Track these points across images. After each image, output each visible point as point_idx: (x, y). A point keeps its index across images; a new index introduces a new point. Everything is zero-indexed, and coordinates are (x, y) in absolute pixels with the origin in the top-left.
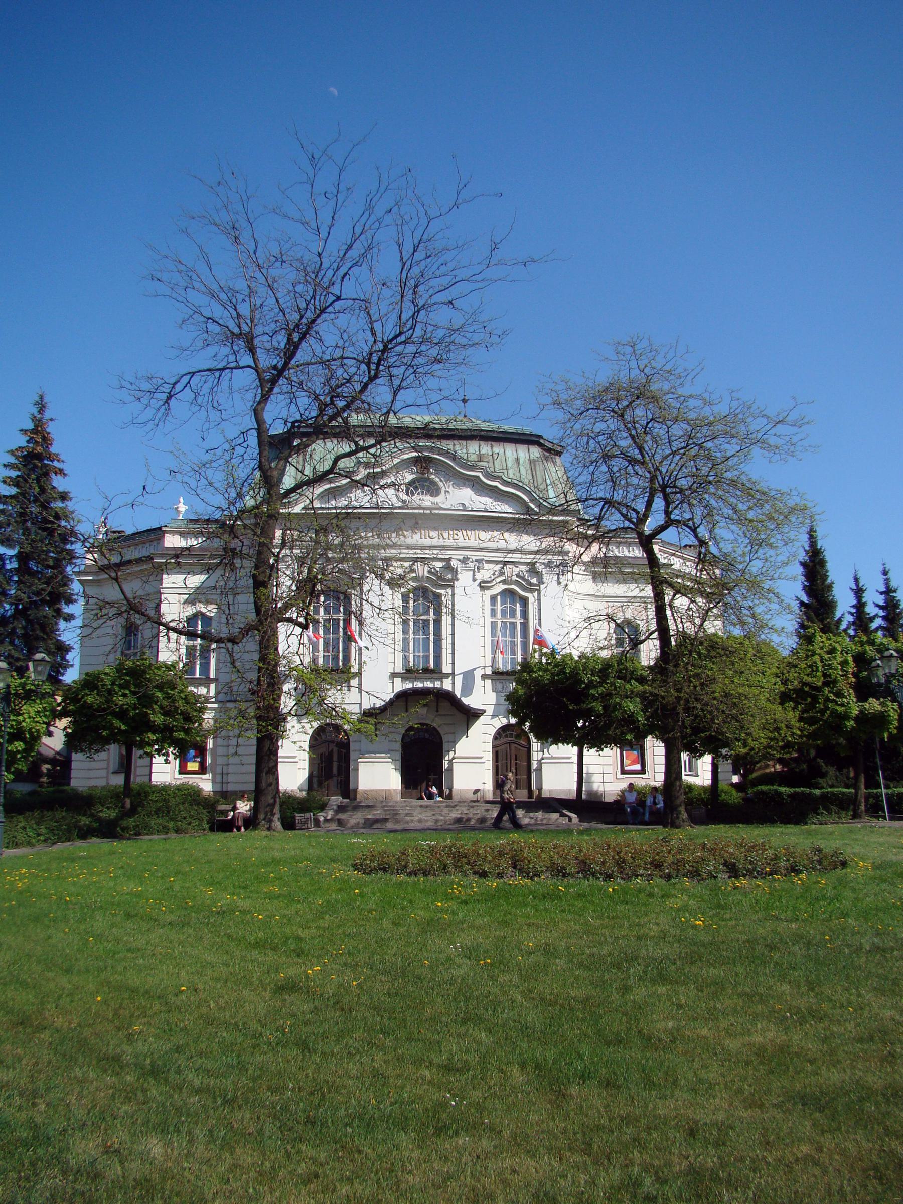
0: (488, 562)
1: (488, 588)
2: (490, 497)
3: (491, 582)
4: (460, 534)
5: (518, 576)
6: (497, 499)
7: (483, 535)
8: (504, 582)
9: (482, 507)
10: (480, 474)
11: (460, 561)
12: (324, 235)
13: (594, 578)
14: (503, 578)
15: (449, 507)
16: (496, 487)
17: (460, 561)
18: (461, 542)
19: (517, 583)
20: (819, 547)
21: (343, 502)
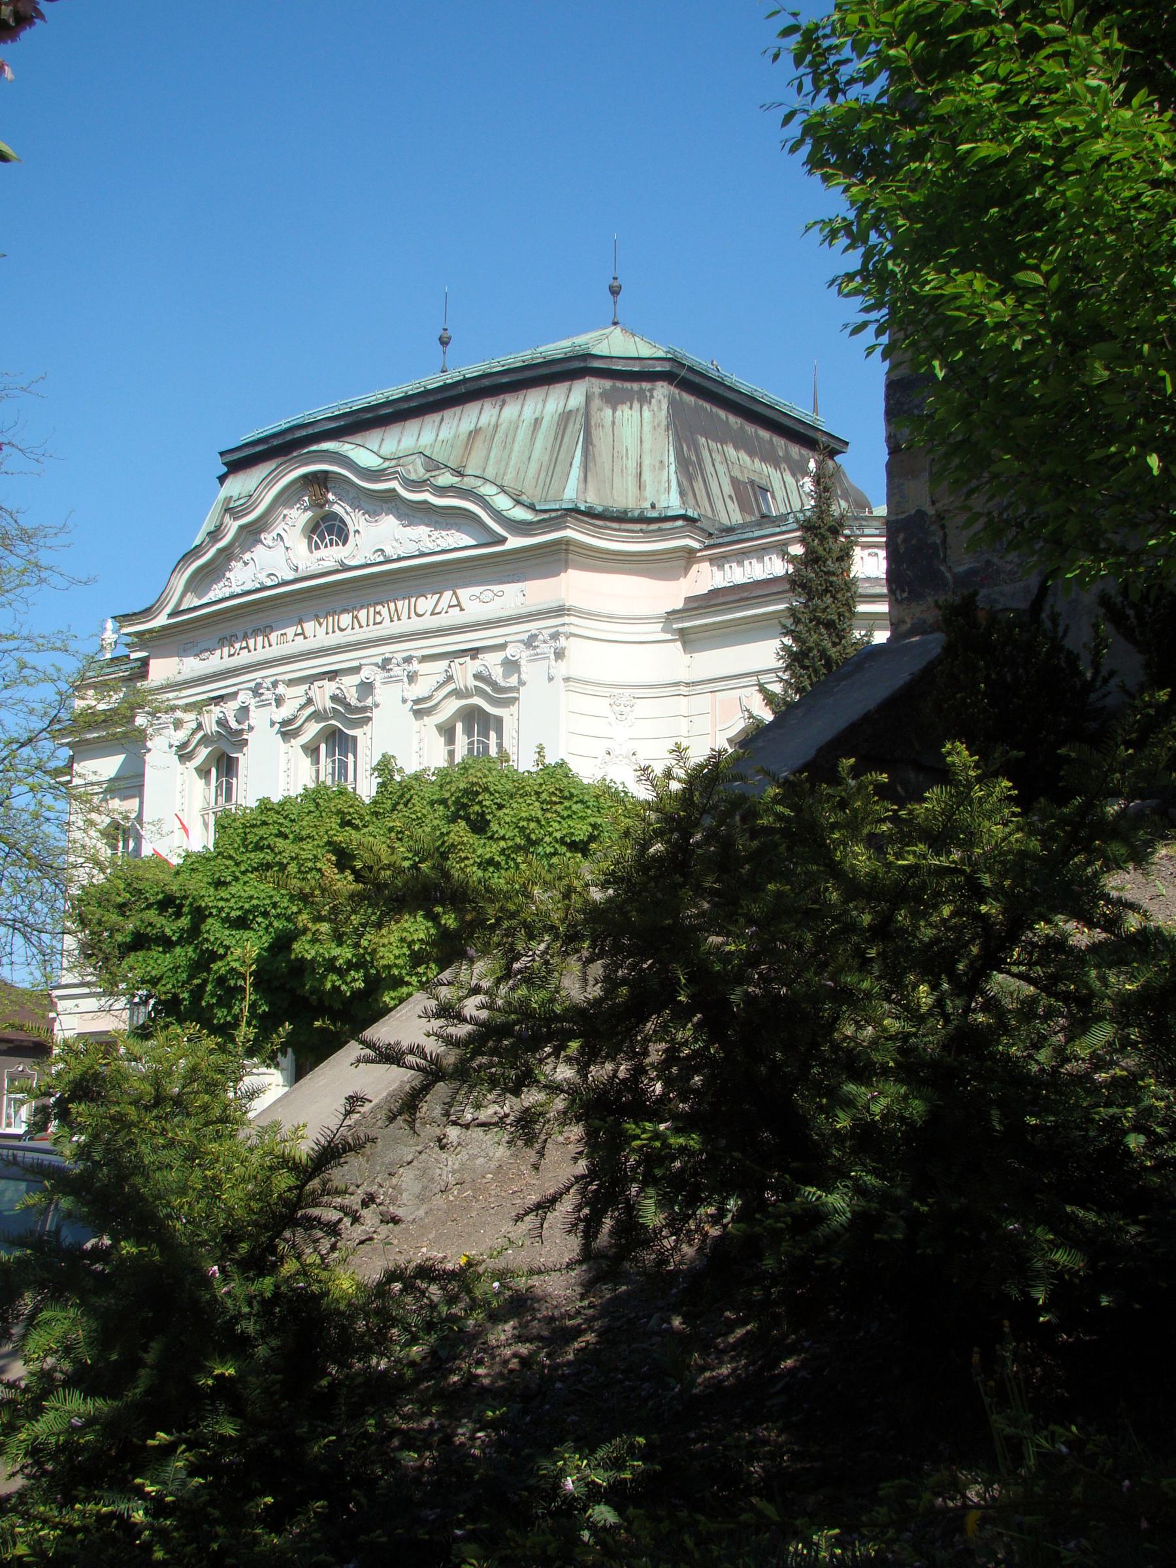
0: (425, 659)
1: (428, 712)
2: (428, 525)
3: (430, 697)
4: (385, 611)
5: (477, 677)
6: (437, 525)
7: (425, 604)
8: (457, 694)
9: (412, 549)
10: (394, 484)
11: (376, 665)
12: (727, 499)
13: (685, 645)
14: (311, 709)
15: (362, 562)
16: (426, 502)
17: (376, 665)
18: (389, 628)
19: (480, 692)
20: (643, 793)
21: (217, 591)
